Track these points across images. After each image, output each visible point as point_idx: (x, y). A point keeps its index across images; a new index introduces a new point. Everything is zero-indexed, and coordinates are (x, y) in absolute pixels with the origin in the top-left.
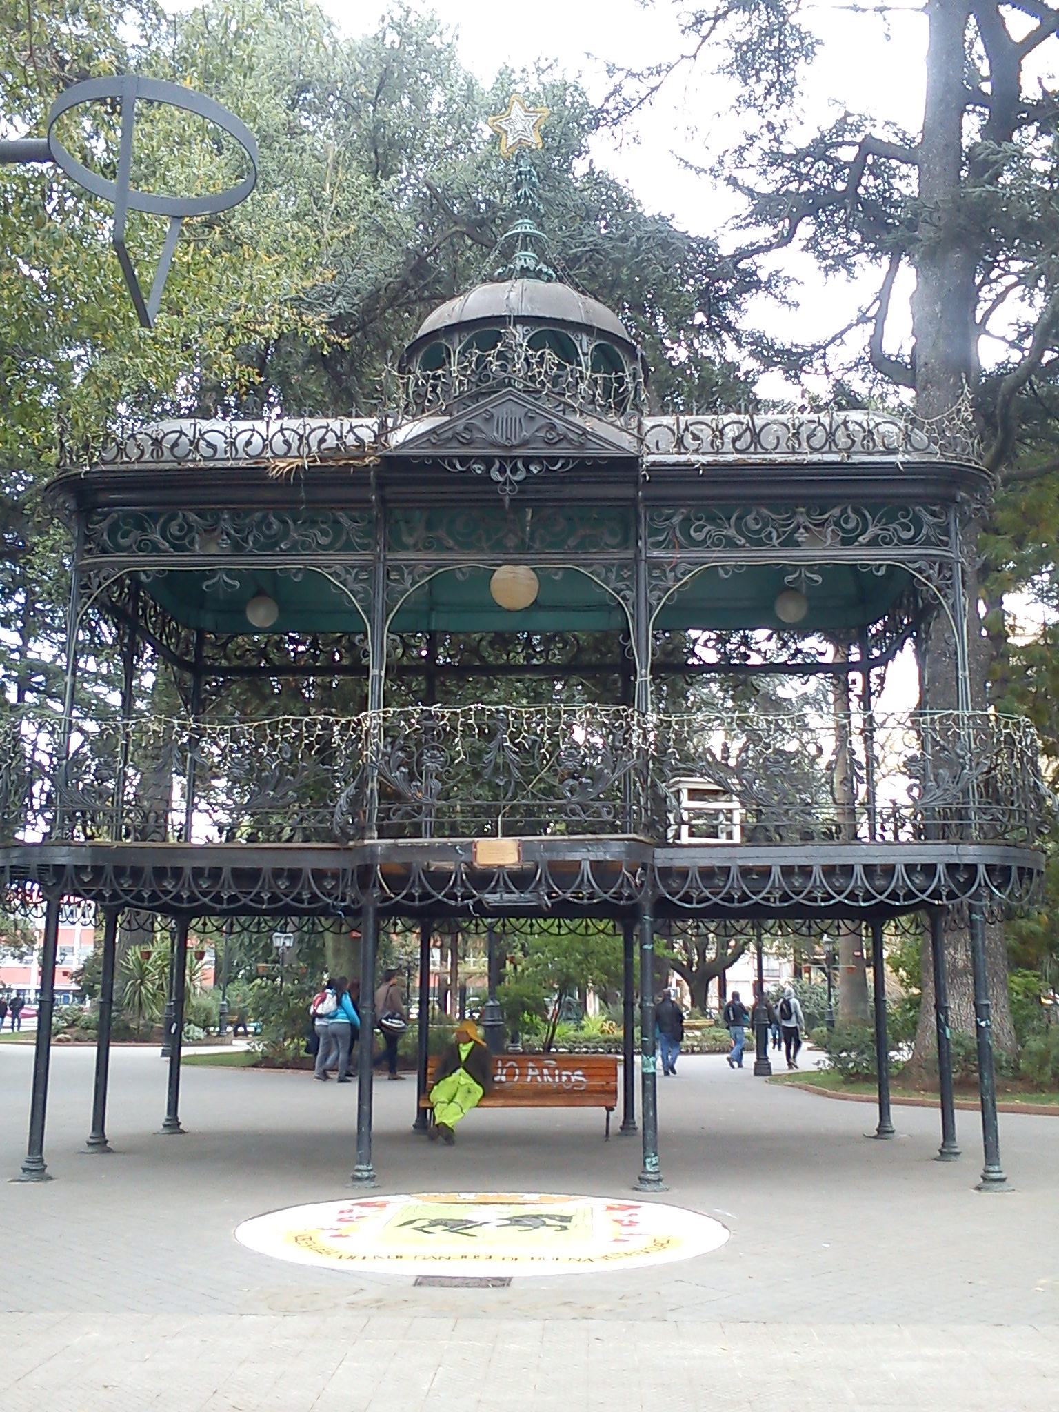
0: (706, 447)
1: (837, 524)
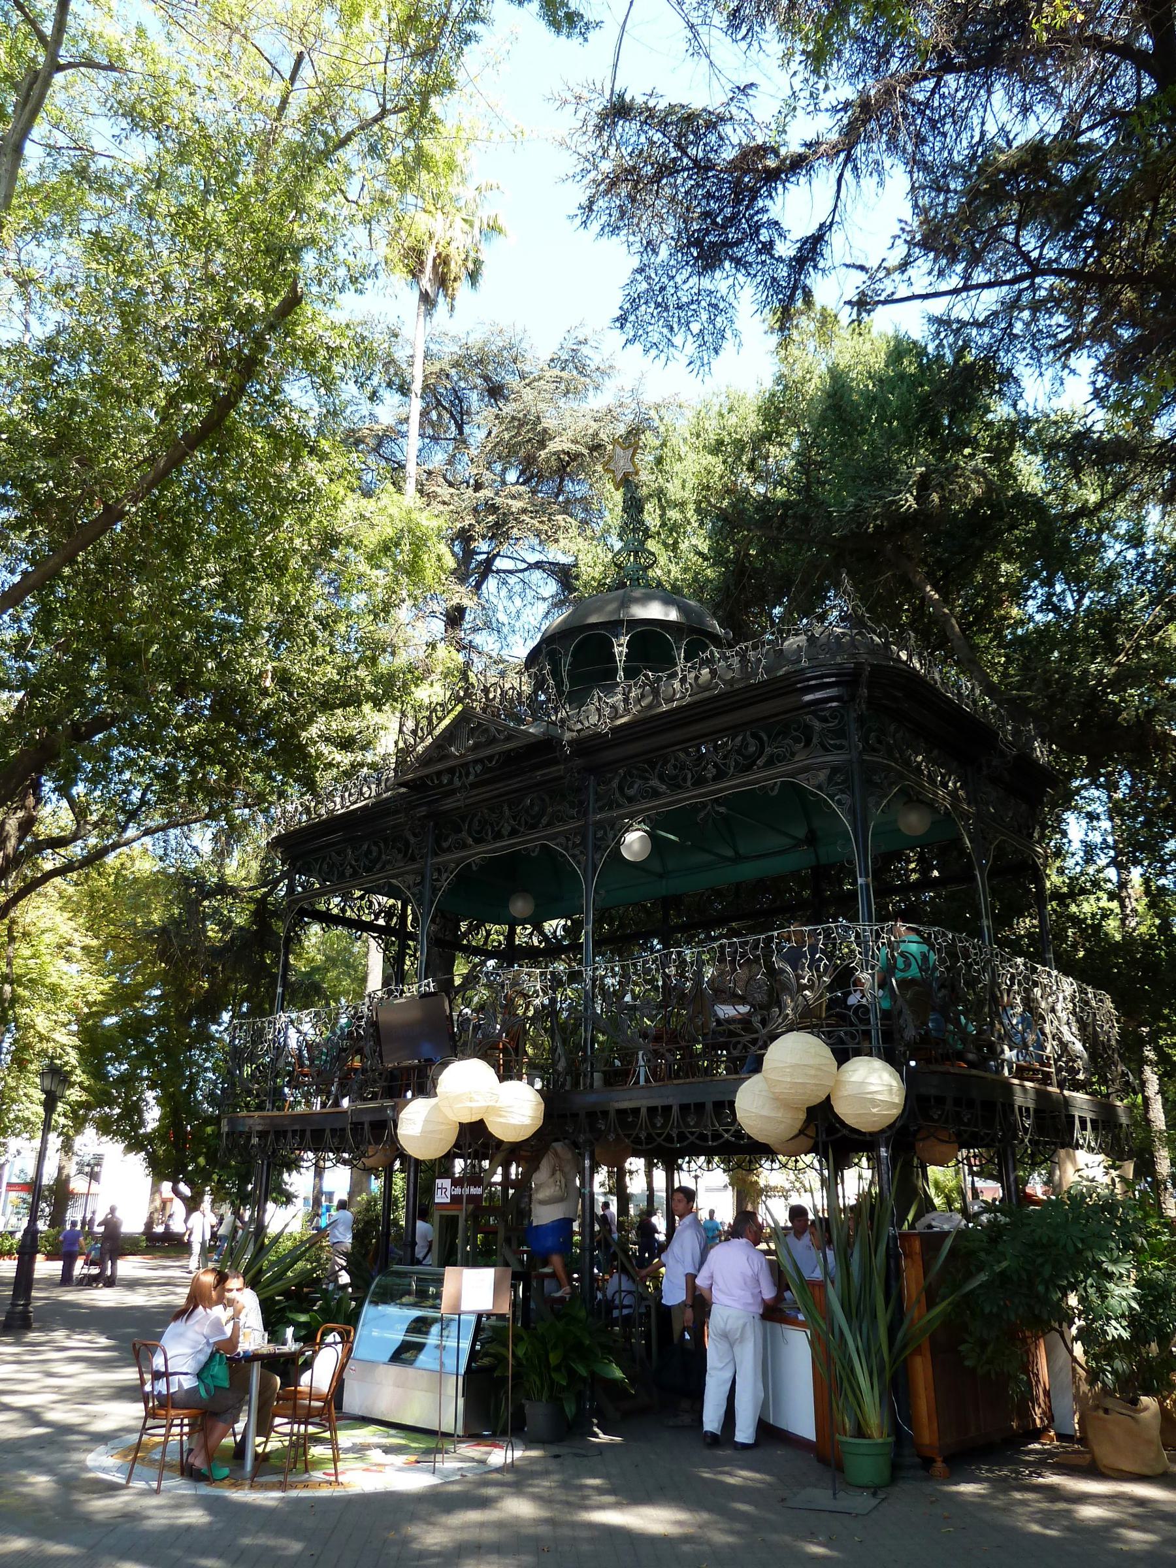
1: (739, 752)
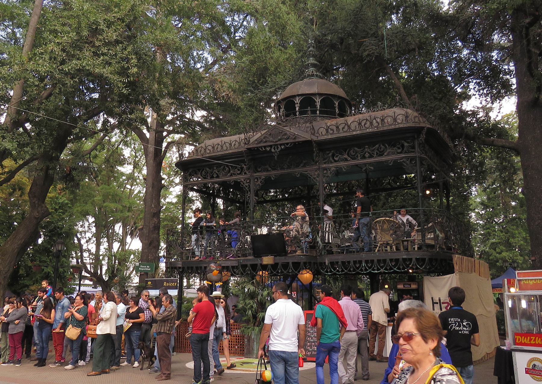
0: (335, 132)
1: (378, 150)
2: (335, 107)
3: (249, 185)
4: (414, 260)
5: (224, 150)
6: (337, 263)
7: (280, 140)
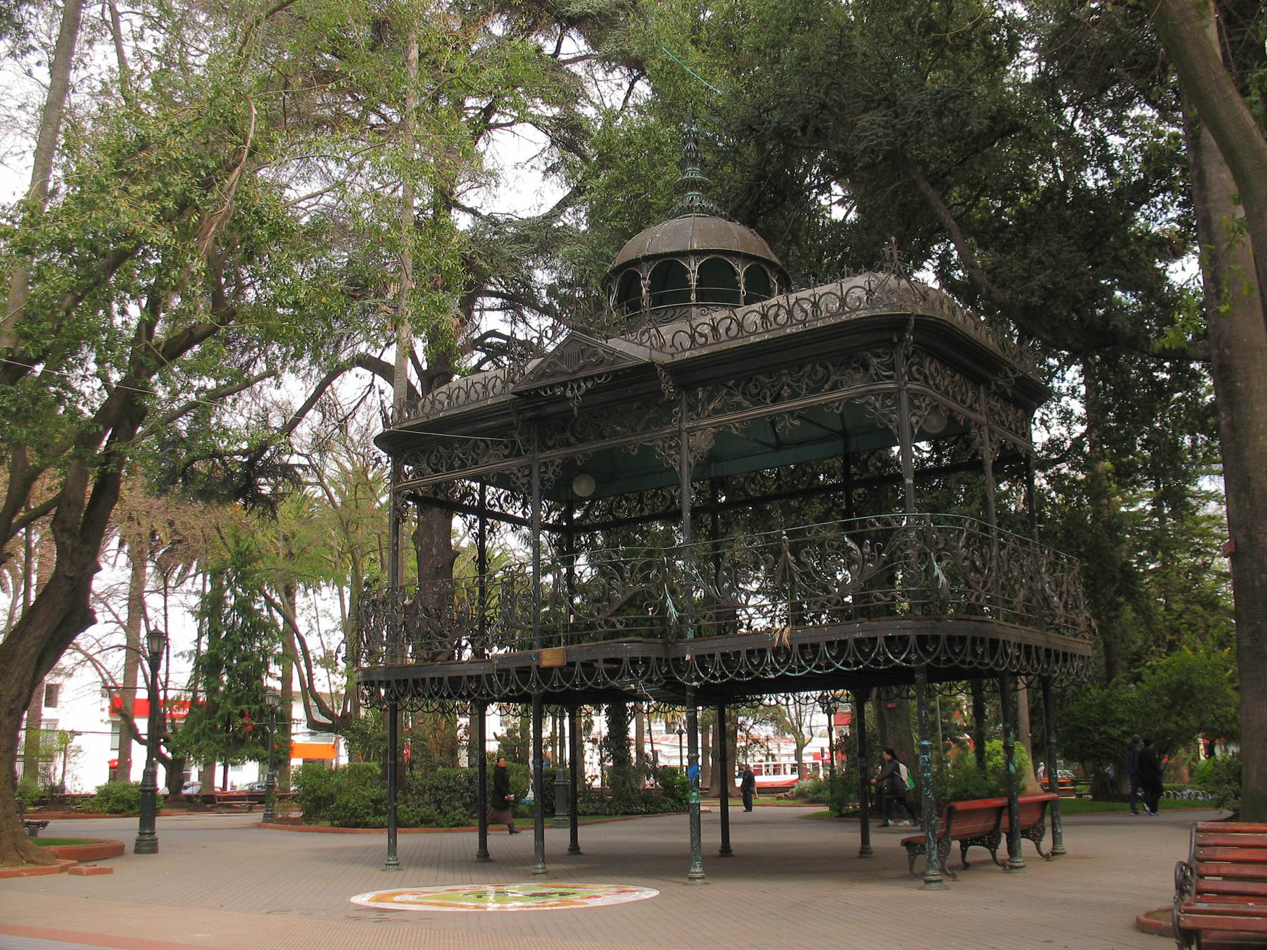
0: (710, 340)
1: (809, 377)
2: (737, 283)
3: (529, 482)
4: (881, 641)
5: (473, 402)
6: (712, 656)
7: (582, 369)
